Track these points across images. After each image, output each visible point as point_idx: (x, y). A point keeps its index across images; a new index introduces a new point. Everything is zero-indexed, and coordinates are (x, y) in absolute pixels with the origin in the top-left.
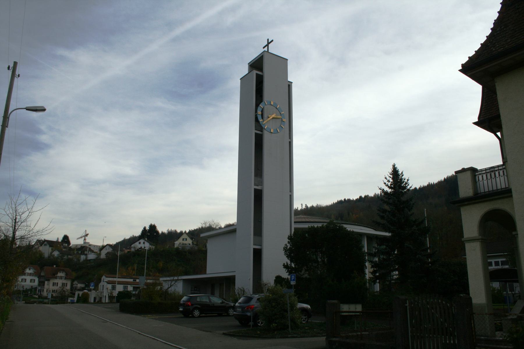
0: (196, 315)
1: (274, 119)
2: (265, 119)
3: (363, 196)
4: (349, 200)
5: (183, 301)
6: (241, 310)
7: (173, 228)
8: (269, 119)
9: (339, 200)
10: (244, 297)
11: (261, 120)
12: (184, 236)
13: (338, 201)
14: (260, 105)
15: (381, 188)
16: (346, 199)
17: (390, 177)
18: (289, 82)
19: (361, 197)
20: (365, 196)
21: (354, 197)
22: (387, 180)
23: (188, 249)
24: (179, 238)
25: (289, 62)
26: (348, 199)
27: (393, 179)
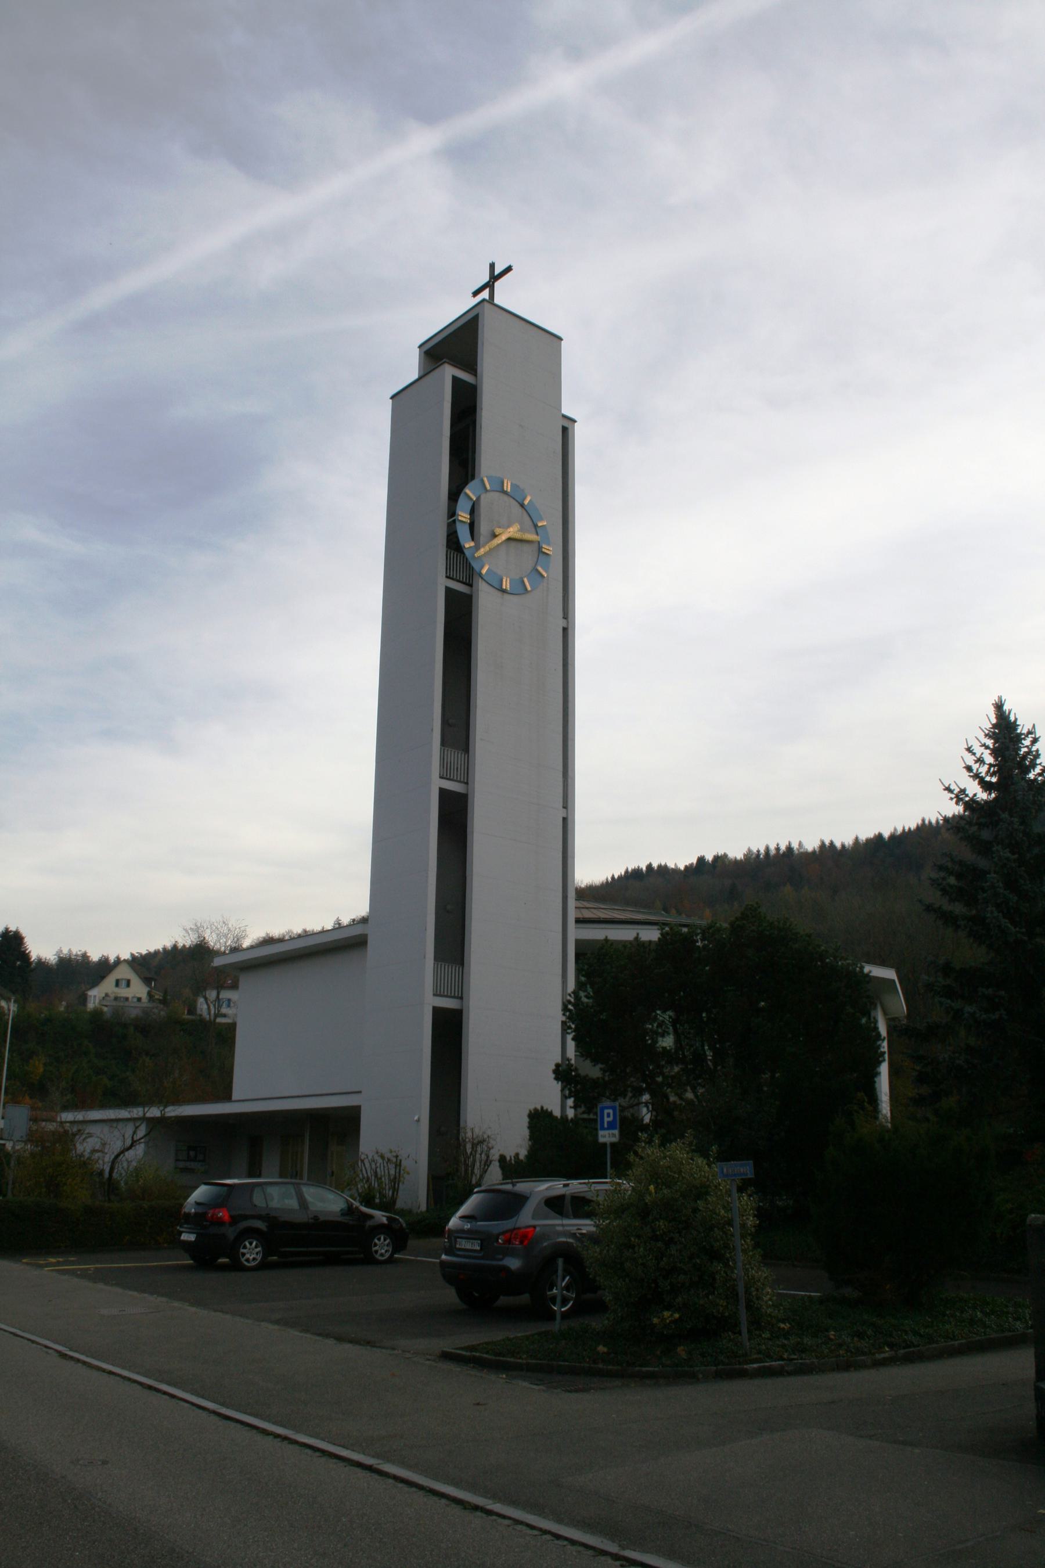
0: (248, 1260)
1: (513, 544)
2: (482, 539)
3: (709, 858)
4: (663, 870)
5: (198, 1204)
6: (478, 1248)
7: (74, 947)
8: (497, 541)
9: (630, 870)
10: (481, 1195)
11: (468, 544)
12: (124, 972)
13: (627, 872)
14: (467, 490)
15: (952, 787)
16: (655, 865)
17: (987, 747)
18: (564, 416)
19: (701, 860)
20: (717, 858)
21: (681, 859)
22: (974, 758)
23: (133, 1016)
24: (103, 978)
25: (567, 348)
26: (660, 866)
27: (995, 752)
